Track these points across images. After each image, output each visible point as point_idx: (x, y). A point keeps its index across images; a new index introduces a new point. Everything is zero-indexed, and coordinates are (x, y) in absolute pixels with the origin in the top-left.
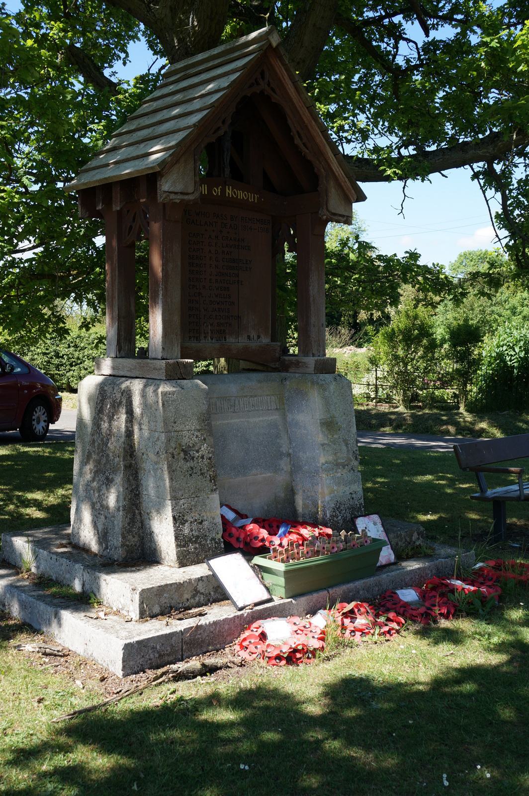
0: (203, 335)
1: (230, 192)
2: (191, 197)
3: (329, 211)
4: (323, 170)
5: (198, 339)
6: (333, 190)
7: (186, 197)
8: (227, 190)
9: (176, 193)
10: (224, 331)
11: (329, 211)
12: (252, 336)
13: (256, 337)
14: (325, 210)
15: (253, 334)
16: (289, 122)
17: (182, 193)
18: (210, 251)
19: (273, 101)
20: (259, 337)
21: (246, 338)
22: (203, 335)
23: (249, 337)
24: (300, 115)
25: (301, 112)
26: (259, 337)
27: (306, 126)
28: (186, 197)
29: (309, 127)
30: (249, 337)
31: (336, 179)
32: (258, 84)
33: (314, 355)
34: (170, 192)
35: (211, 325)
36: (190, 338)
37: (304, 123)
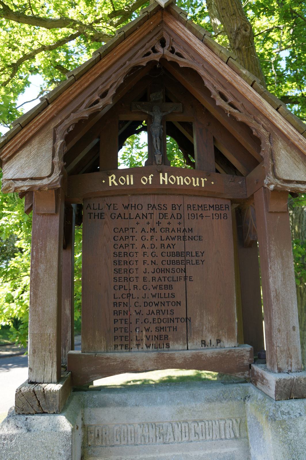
0: (135, 342)
1: (166, 180)
2: (45, 182)
3: (279, 179)
4: (263, 131)
5: (128, 348)
6: (283, 152)
7: (38, 183)
8: (161, 178)
9: (24, 180)
10: (166, 337)
11: (279, 179)
12: (208, 341)
13: (214, 342)
14: (271, 178)
15: (210, 338)
16: (206, 83)
17: (32, 179)
18: (143, 246)
19: (181, 66)
20: (219, 341)
21: (200, 343)
22: (135, 342)
23: (204, 343)
24: (219, 73)
25: (220, 70)
26: (219, 341)
27: (230, 84)
28: (38, 183)
29: (235, 84)
30: (204, 343)
31: (285, 138)
32: (155, 51)
33: (280, 371)
34: (14, 180)
35: (147, 330)
36: (116, 346)
37: (227, 80)
